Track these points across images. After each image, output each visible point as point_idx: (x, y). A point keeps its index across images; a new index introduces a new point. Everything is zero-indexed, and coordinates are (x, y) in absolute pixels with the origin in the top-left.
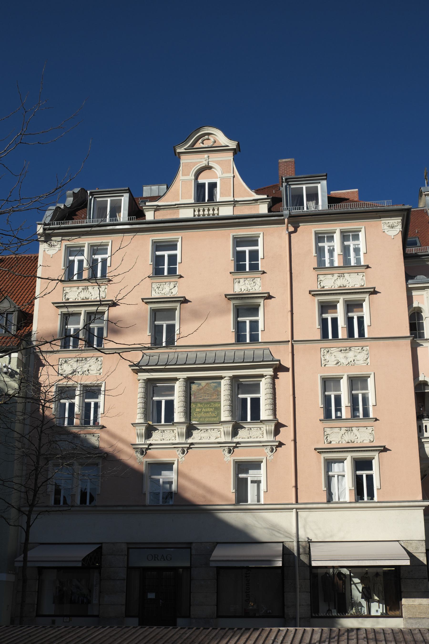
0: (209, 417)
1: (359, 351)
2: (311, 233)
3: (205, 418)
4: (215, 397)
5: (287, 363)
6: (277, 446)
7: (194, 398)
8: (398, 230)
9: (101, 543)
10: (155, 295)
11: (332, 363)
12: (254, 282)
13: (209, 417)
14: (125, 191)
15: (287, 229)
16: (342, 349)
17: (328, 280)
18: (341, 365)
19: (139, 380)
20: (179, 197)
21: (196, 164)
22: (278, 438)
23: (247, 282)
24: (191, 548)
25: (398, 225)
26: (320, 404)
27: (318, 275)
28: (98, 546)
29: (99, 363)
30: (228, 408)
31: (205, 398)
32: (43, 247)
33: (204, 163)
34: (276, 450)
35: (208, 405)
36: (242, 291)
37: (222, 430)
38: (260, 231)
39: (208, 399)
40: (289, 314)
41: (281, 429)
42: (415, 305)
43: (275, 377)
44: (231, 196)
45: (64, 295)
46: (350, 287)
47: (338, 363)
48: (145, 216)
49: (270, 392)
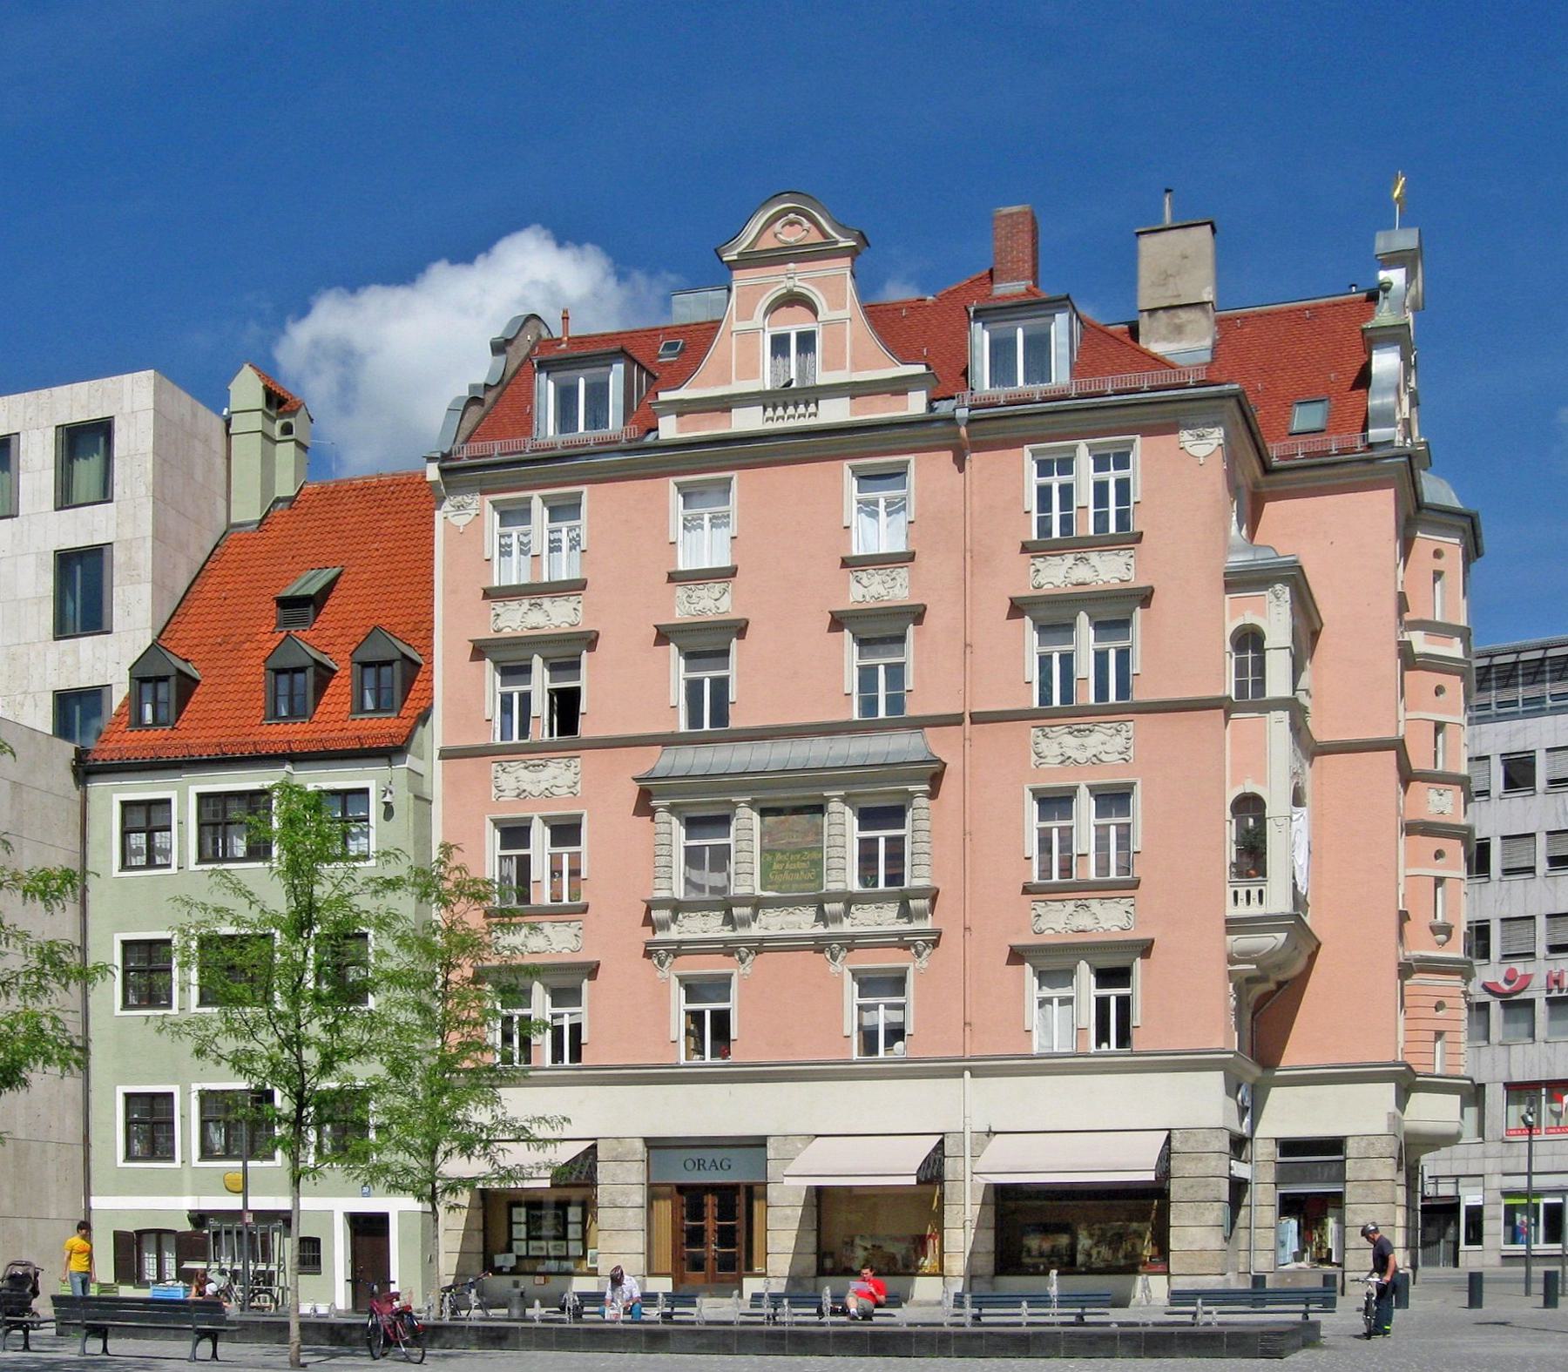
0: (798, 882)
4: (809, 839)
8: (1215, 443)
9: (595, 1139)
11: (1052, 761)
13: (798, 882)
28: (590, 1143)
35: (798, 856)
44: (851, 415)
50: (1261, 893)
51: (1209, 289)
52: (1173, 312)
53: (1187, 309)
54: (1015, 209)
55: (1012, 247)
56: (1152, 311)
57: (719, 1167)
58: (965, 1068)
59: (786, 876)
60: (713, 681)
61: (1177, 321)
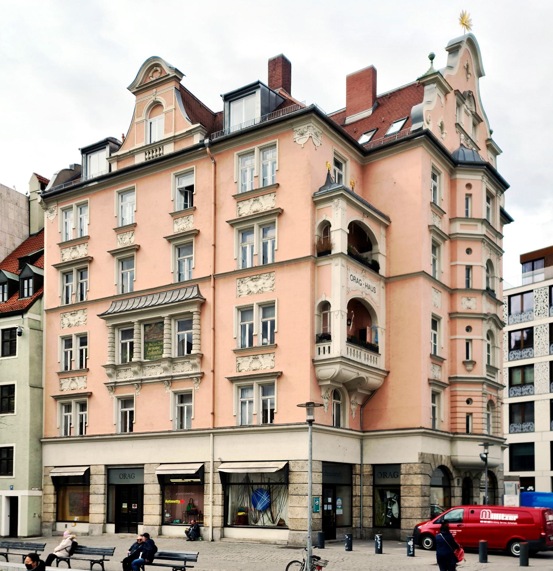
0: (157, 355)
3: (154, 355)
9: (89, 466)
10: (119, 246)
28: (87, 468)
46: (263, 211)
50: (329, 347)
58: (210, 433)
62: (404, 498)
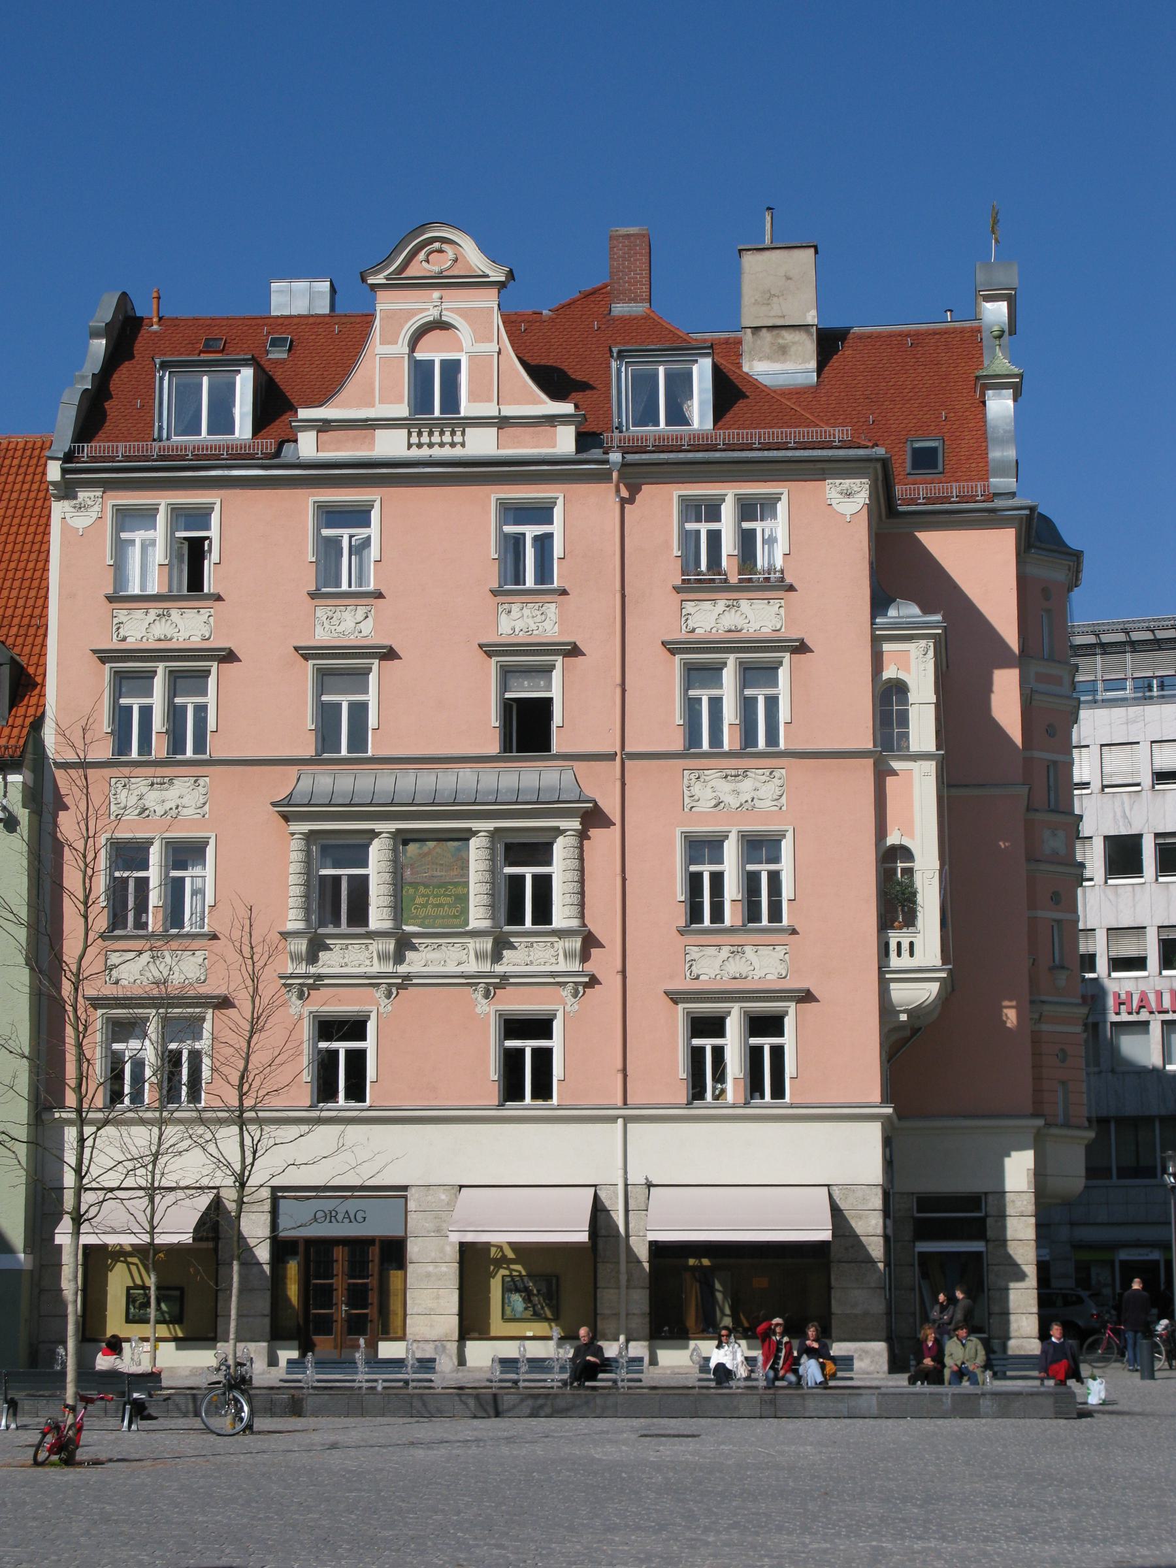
0: (443, 917)
1: (764, 778)
2: (671, 499)
5: (611, 807)
6: (587, 985)
7: (411, 874)
11: (705, 805)
12: (542, 614)
13: (443, 917)
14: (245, 363)
15: (618, 491)
16: (729, 772)
17: (704, 612)
18: (725, 809)
19: (293, 834)
20: (374, 397)
21: (416, 315)
22: (589, 967)
23: (526, 612)
24: (405, 1197)
25: (860, 489)
26: (680, 893)
27: (682, 601)
29: (202, 790)
30: (485, 900)
31: (435, 873)
32: (59, 509)
33: (431, 314)
34: (584, 992)
36: (517, 632)
37: (471, 946)
38: (557, 492)
39: (442, 876)
40: (618, 691)
41: (594, 951)
42: (889, 673)
43: (583, 835)
45: (115, 628)
47: (719, 803)
48: (296, 412)
49: (574, 866)
50: (911, 944)
51: (814, 313)
52: (775, 332)
53: (791, 330)
54: (633, 230)
55: (629, 268)
56: (756, 329)
57: (353, 1219)
59: (430, 910)
60: (352, 705)
61: (781, 341)
62: (996, 1268)
